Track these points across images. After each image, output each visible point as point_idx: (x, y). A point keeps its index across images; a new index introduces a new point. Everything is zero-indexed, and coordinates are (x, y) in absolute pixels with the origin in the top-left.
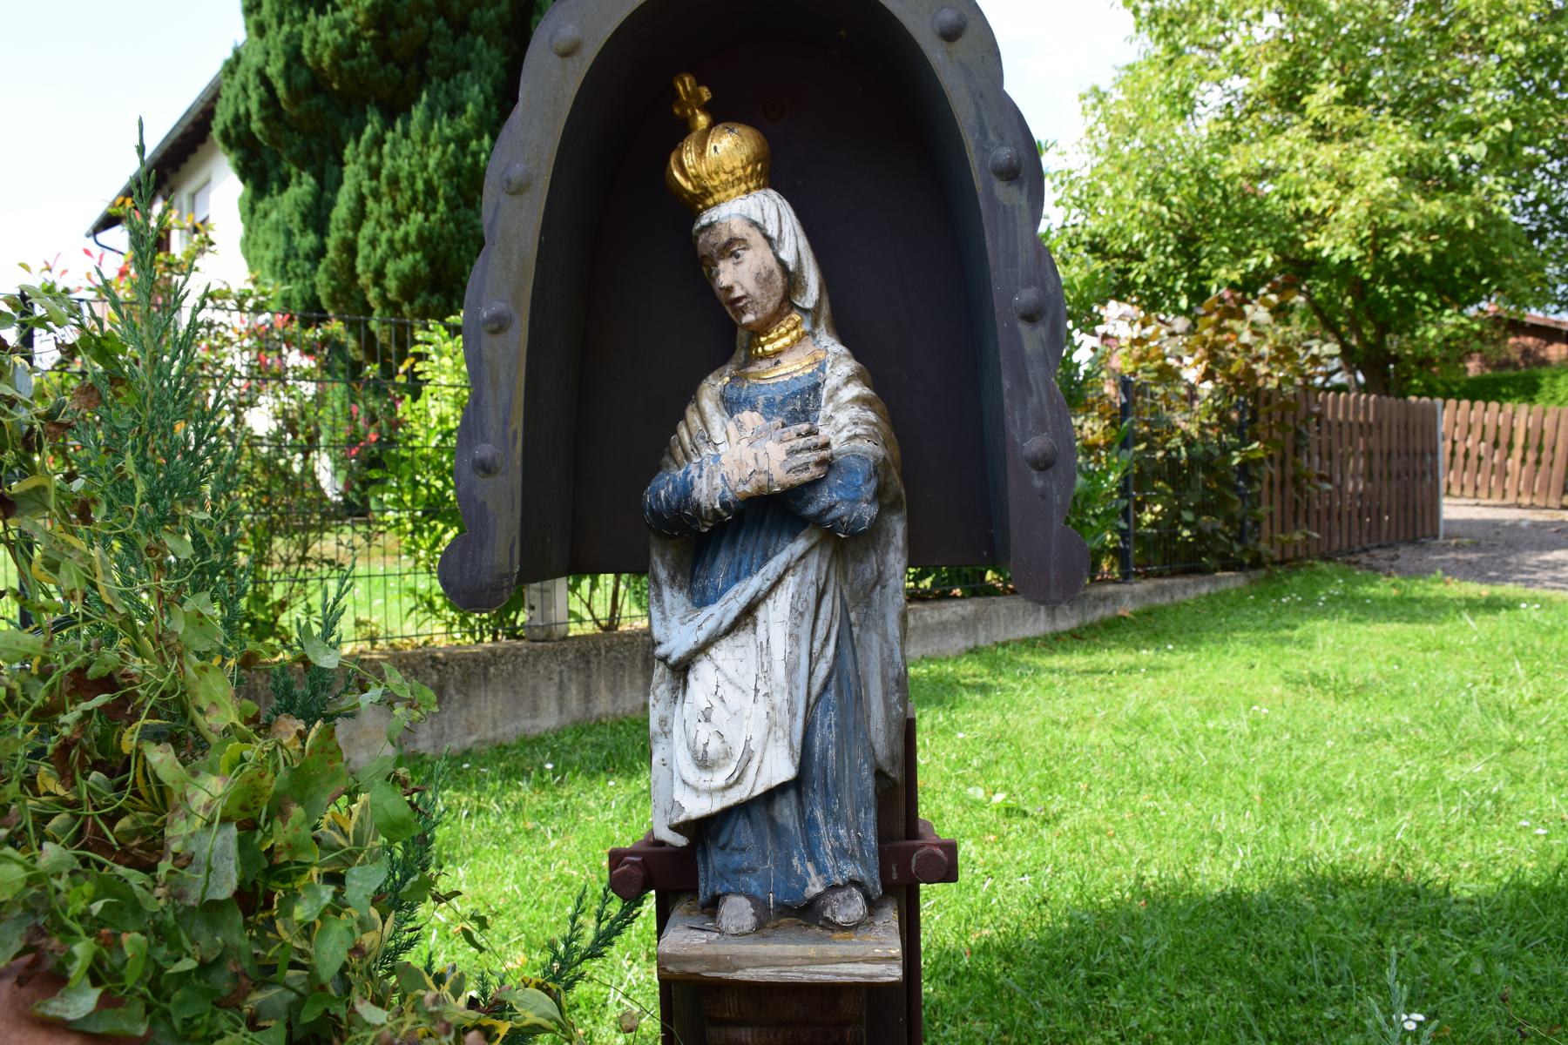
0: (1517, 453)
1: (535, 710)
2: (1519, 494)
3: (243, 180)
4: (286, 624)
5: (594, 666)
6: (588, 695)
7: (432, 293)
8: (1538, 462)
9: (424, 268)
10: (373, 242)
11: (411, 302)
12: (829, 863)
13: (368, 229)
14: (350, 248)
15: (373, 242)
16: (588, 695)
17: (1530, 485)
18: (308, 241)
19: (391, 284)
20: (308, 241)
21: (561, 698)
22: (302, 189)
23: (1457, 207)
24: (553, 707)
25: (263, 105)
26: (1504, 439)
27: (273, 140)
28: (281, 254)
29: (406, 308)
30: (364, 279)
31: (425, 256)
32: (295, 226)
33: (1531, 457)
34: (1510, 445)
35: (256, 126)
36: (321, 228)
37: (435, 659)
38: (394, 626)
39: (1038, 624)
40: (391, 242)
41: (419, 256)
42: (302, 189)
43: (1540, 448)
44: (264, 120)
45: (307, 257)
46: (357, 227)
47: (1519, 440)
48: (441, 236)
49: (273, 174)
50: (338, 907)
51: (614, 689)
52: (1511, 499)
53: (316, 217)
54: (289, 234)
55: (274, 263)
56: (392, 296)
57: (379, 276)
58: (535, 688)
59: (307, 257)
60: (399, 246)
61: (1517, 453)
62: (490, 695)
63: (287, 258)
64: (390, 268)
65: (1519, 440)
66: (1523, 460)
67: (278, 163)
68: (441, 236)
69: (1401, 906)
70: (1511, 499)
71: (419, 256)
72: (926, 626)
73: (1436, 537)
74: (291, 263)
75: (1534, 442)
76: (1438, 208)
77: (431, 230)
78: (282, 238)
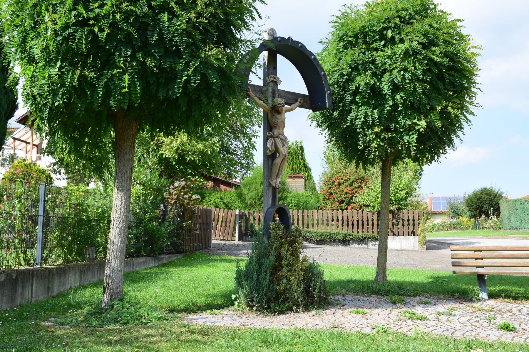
0: (220, 223)
2: (220, 236)
3: (396, 282)
4: (202, 322)
8: (226, 226)
12: (350, 39)
17: (223, 233)
23: (205, 146)
26: (216, 219)
33: (224, 225)
34: (218, 221)
43: (226, 222)
47: (220, 219)
50: (69, 329)
52: (217, 237)
61: (220, 223)
62: (459, 133)
65: (220, 219)
66: (221, 226)
69: (318, 308)
70: (217, 237)
73: (210, 247)
75: (225, 220)
76: (200, 146)
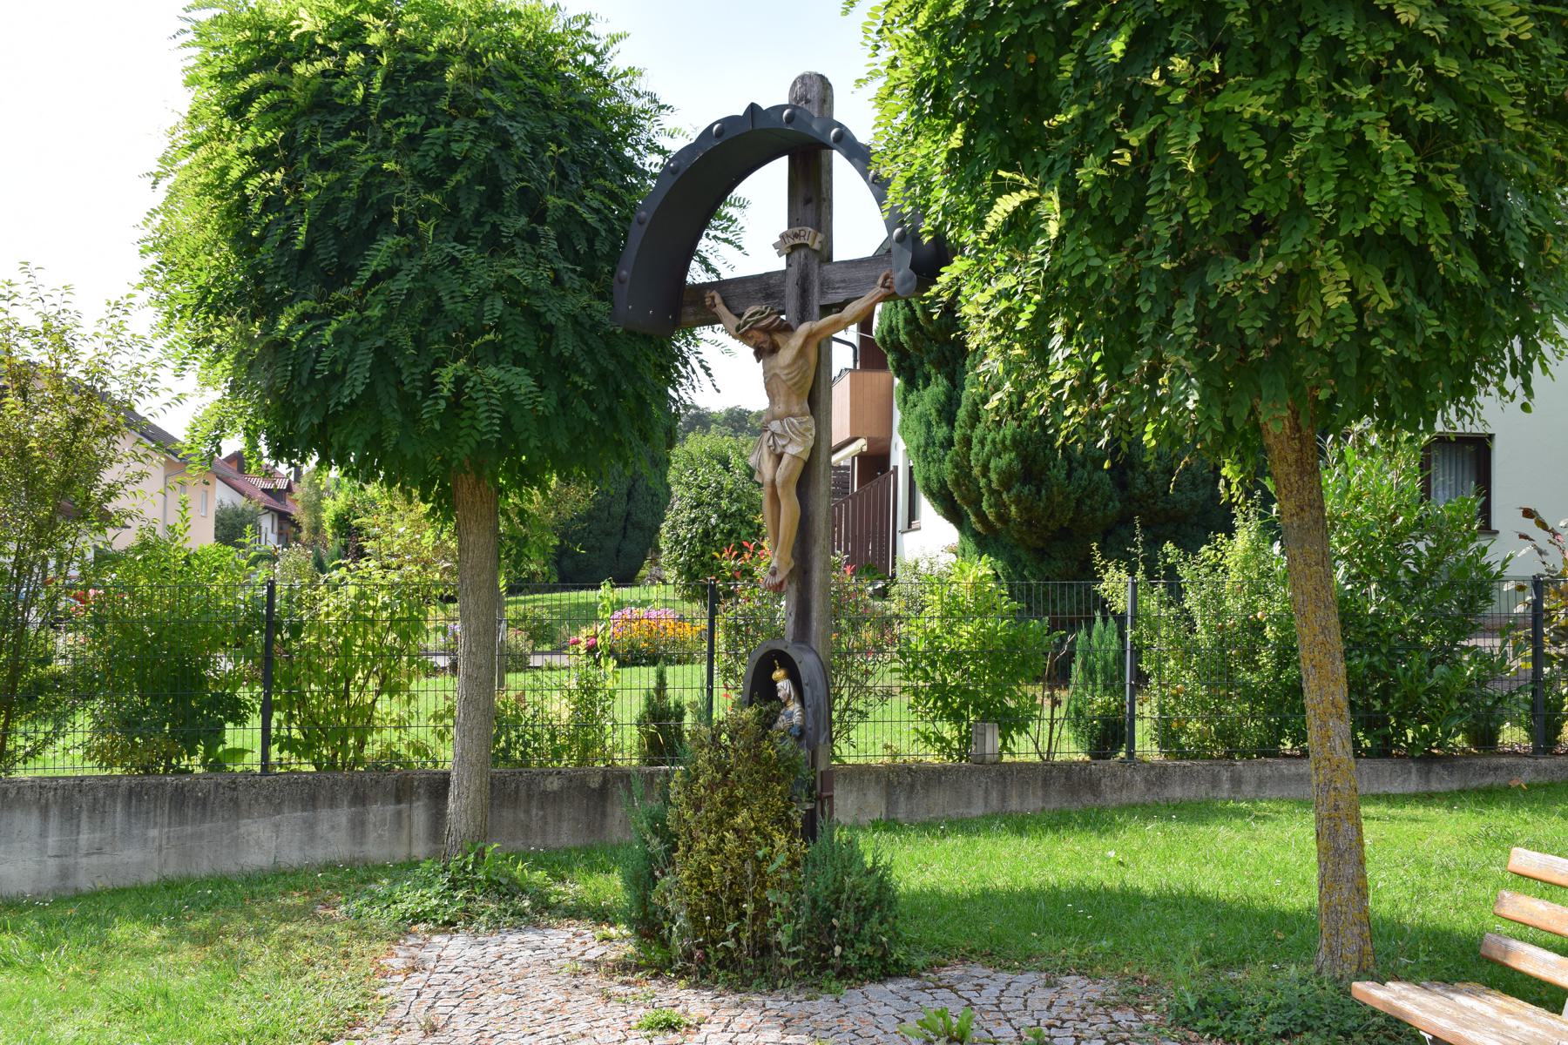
1: (969, 804)
5: (1008, 781)
6: (1004, 798)
7: (1024, 484)
9: (1017, 466)
10: (982, 442)
11: (1008, 491)
13: (979, 431)
14: (967, 441)
15: (982, 442)
16: (1004, 798)
18: (941, 432)
19: (993, 476)
20: (941, 432)
21: (986, 799)
22: (937, 388)
24: (981, 803)
25: (907, 321)
27: (915, 346)
28: (923, 442)
29: (1005, 496)
30: (976, 471)
31: (1018, 455)
32: (934, 417)
35: (903, 338)
36: (950, 419)
37: (910, 769)
38: (904, 749)
39: (1413, 784)
40: (994, 441)
41: (1013, 455)
42: (937, 388)
44: (907, 334)
45: (942, 445)
46: (973, 427)
48: (1030, 439)
49: (918, 373)
51: (1022, 796)
53: (947, 411)
54: (929, 425)
55: (918, 447)
56: (994, 485)
57: (985, 470)
58: (969, 791)
59: (942, 445)
60: (999, 446)
63: (927, 445)
64: (992, 465)
67: (922, 363)
68: (1030, 439)
71: (1013, 455)
72: (1282, 776)
74: (930, 450)
77: (1021, 435)
78: (924, 429)
